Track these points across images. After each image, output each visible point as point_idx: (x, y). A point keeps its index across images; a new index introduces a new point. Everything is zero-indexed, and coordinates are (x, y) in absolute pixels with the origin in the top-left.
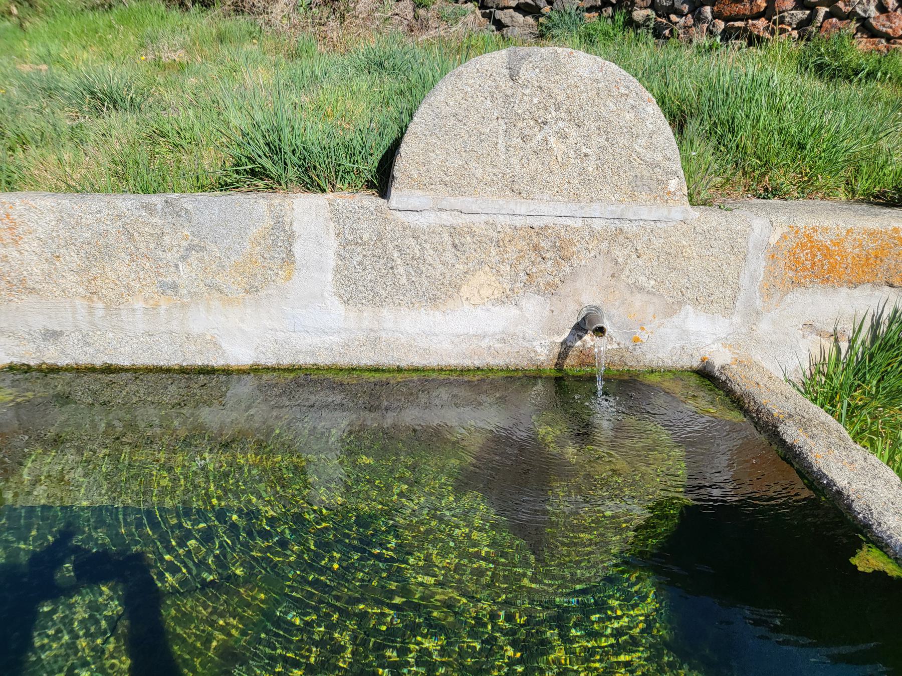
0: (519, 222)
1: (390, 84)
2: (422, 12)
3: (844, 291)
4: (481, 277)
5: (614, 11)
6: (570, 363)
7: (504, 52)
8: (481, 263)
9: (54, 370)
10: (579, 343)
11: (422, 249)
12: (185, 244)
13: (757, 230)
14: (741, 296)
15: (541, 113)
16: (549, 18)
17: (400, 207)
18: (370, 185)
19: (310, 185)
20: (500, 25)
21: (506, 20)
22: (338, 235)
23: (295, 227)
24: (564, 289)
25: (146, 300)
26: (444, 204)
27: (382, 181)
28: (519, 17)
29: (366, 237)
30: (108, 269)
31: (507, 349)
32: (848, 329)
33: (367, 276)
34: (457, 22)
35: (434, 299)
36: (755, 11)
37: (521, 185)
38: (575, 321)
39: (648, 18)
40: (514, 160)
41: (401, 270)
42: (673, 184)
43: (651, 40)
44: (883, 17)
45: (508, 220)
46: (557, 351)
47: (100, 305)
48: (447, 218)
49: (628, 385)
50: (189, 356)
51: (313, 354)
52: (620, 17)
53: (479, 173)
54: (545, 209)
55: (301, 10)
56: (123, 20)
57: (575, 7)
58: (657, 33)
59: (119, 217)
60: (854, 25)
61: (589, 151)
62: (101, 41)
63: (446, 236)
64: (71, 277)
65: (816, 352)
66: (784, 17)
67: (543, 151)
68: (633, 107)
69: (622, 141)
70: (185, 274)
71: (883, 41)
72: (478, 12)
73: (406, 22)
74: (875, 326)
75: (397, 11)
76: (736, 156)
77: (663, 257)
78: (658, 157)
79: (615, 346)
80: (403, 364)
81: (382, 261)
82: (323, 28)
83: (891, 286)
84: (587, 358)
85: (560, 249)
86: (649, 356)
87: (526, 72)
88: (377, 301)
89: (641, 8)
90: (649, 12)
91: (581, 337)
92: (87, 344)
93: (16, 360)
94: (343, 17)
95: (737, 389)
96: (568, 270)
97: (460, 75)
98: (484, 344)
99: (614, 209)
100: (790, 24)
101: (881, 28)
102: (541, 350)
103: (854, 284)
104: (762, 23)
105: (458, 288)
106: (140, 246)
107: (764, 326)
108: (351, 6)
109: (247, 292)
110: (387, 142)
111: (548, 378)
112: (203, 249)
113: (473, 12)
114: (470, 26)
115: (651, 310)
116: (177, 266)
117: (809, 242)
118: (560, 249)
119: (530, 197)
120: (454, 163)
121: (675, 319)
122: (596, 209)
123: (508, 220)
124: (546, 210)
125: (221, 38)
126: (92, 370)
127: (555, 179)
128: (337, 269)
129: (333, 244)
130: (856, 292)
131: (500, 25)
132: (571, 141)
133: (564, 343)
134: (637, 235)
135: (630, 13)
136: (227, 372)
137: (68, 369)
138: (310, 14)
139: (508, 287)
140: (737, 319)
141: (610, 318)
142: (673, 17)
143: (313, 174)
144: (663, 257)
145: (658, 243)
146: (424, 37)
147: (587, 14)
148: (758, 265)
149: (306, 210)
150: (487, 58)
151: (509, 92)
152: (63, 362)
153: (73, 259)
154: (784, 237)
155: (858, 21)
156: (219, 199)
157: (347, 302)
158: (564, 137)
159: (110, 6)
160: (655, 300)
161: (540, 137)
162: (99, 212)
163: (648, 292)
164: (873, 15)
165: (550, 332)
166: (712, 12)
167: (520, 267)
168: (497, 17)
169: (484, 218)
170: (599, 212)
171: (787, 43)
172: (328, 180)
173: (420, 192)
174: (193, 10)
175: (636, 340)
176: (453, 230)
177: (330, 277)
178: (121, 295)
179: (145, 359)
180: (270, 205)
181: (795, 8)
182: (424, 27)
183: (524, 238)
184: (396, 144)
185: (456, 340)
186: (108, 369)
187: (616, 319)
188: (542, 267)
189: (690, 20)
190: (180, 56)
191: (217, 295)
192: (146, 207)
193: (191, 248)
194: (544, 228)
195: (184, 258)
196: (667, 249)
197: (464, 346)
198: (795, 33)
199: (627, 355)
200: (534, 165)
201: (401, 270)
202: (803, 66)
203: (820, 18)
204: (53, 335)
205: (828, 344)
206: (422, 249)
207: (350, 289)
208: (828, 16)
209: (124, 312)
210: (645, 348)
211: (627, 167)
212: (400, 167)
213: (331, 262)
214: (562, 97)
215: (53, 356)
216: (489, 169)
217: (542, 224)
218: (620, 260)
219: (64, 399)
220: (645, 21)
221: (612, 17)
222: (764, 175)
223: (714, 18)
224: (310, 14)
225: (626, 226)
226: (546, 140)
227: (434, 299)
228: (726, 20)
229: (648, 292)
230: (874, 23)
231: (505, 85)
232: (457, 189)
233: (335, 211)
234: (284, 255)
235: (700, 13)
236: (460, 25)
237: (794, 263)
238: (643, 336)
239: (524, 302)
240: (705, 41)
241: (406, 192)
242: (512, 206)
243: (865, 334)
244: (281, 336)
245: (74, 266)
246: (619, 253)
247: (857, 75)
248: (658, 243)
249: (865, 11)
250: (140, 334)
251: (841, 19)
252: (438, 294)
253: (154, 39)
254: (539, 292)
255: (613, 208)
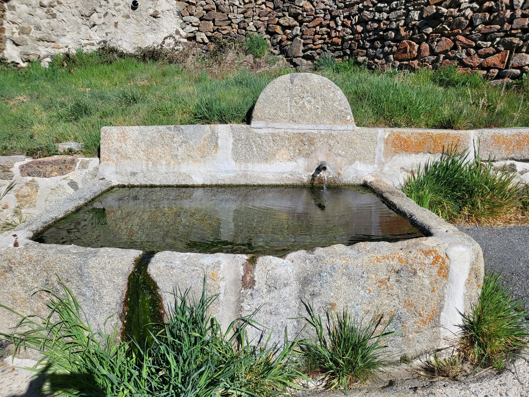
0: (295, 131)
1: (247, 90)
2: (257, 60)
3: (413, 155)
4: (283, 151)
5: (349, 57)
6: (316, 182)
7: (289, 75)
8: (283, 146)
9: (133, 186)
10: (318, 175)
11: (262, 142)
12: (181, 141)
13: (380, 134)
14: (376, 157)
15: (302, 94)
16: (319, 61)
17: (255, 127)
18: (243, 121)
19: (223, 121)
20: (295, 65)
21: (298, 63)
22: (233, 137)
23: (219, 134)
24: (313, 155)
25: (166, 161)
26: (269, 126)
27: (248, 119)
28: (305, 61)
29: (243, 138)
30: (154, 150)
31: (293, 178)
32: (415, 169)
33: (243, 151)
34: (274, 64)
35: (267, 159)
36: (412, 56)
37: (296, 119)
38: (317, 167)
39: (365, 61)
40: (293, 110)
41: (255, 149)
42: (349, 118)
43: (366, 70)
44: (469, 58)
45: (292, 131)
46: (311, 178)
47: (151, 163)
48: (271, 131)
49: (336, 188)
50: (180, 181)
51: (224, 180)
52: (352, 61)
53: (281, 115)
54: (304, 127)
55: (200, 60)
56: (118, 68)
57: (331, 56)
58: (369, 67)
59: (160, 132)
60: (456, 62)
61: (319, 107)
62: (109, 78)
63: (270, 137)
64: (142, 153)
65: (406, 178)
66: (425, 59)
67: (303, 107)
68: (333, 92)
69: (330, 103)
70: (181, 151)
71: (470, 69)
72: (285, 59)
73: (250, 65)
74: (426, 168)
75: (245, 60)
76: (375, 109)
77: (347, 143)
78: (343, 108)
79: (332, 176)
80: (255, 184)
81: (248, 146)
82: (211, 68)
83: (430, 153)
84: (321, 181)
85: (310, 141)
86: (344, 180)
87: (296, 81)
88: (247, 161)
89: (361, 56)
90: (365, 57)
91: (319, 173)
92: (145, 177)
93: (121, 183)
94: (220, 63)
95: (374, 187)
96: (313, 148)
97: (274, 82)
98: (284, 176)
99: (329, 127)
100: (428, 63)
101: (468, 63)
102: (306, 178)
103: (417, 153)
104: (416, 62)
105: (275, 155)
106: (166, 141)
107: (386, 169)
108: (224, 58)
109: (201, 157)
110: (249, 106)
111: (308, 187)
112: (187, 142)
113: (282, 59)
114: (281, 66)
115: (344, 162)
116: (178, 149)
117: (398, 137)
118: (310, 141)
119: (299, 123)
120: (273, 112)
121: (352, 166)
122: (322, 127)
123: (292, 131)
124: (304, 127)
125: (164, 75)
126: (146, 186)
127: (307, 117)
128: (233, 149)
129: (231, 140)
130: (418, 156)
131: (295, 65)
132: (313, 103)
133: (313, 175)
134: (337, 135)
135: (356, 58)
136: (193, 187)
137: (137, 186)
138: (204, 62)
139: (292, 155)
140: (376, 166)
141: (329, 166)
142: (376, 60)
143: (224, 118)
144: (347, 143)
145: (345, 138)
146: (259, 71)
147: (336, 59)
148: (381, 146)
149: (223, 130)
150: (283, 76)
151: (291, 88)
152: (136, 184)
153: (143, 147)
154: (389, 135)
155: (458, 60)
156: (192, 127)
157: (236, 161)
158: (310, 102)
159: (111, 62)
160: (345, 159)
161: (302, 102)
162: (153, 130)
163: (343, 156)
164: (464, 57)
165: (308, 171)
166: (394, 57)
167: (296, 148)
168: (294, 61)
169: (283, 130)
170: (323, 128)
171: (428, 71)
172: (229, 119)
173: (261, 122)
174: (149, 62)
175: (339, 174)
176: (273, 135)
177: (230, 152)
178: (158, 159)
179: (165, 183)
180: (210, 127)
181: (430, 55)
182: (259, 66)
183: (297, 137)
184: (254, 105)
185: (274, 174)
186: (152, 186)
187: (331, 166)
188: (304, 147)
189: (384, 61)
190: (146, 83)
191: (191, 159)
192: (168, 128)
193: (183, 142)
194: (305, 134)
195: (180, 146)
196: (348, 140)
197: (277, 177)
198: (431, 66)
199: (336, 179)
200: (300, 112)
201: (255, 149)
202: (434, 81)
203: (441, 59)
204: (134, 174)
205: (410, 175)
206: (262, 142)
207: (237, 157)
208: (444, 58)
209: (158, 166)
210: (342, 177)
211: (332, 112)
212: (256, 112)
213: (231, 146)
214: (309, 89)
215: (133, 181)
216: (284, 113)
217: (303, 132)
218: (332, 145)
219: (136, 198)
220: (363, 62)
221: (348, 60)
222: (391, 119)
223: (395, 60)
224: (204, 62)
225: (333, 132)
226: (304, 104)
227: (266, 159)
228: (400, 61)
229: (343, 156)
230: (465, 61)
231: (289, 85)
232: (274, 121)
233: (232, 129)
234: (214, 144)
235: (388, 58)
236: (276, 65)
237: (394, 145)
238: (342, 172)
239: (298, 160)
240: (390, 70)
241: (257, 122)
242: (293, 126)
243: (422, 170)
244: (213, 174)
245: (143, 149)
246: (331, 142)
247: (457, 84)
248: (345, 138)
249: (461, 56)
250: (162, 174)
251: (450, 60)
252: (267, 158)
253: (133, 76)
254: (303, 157)
255: (328, 126)
